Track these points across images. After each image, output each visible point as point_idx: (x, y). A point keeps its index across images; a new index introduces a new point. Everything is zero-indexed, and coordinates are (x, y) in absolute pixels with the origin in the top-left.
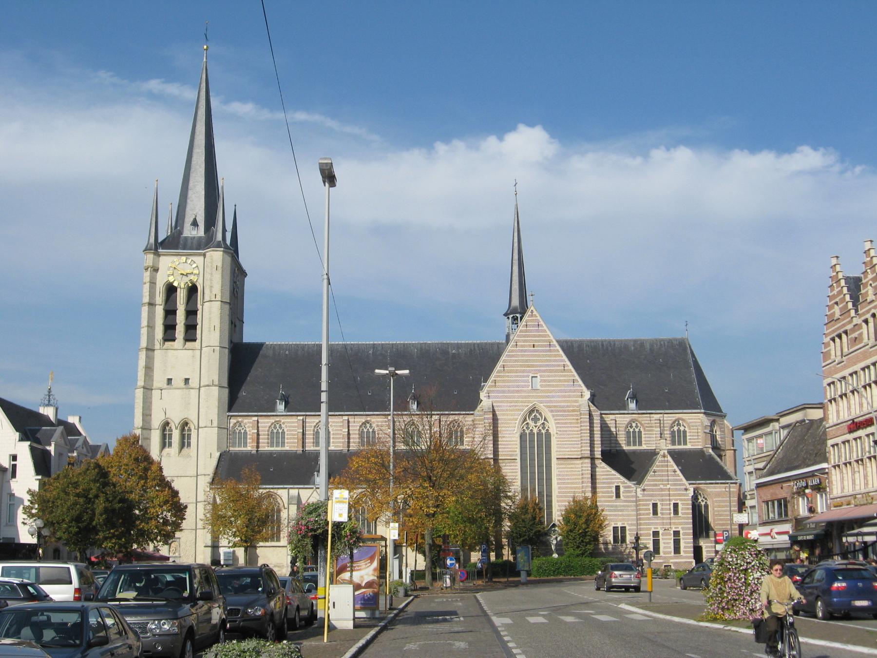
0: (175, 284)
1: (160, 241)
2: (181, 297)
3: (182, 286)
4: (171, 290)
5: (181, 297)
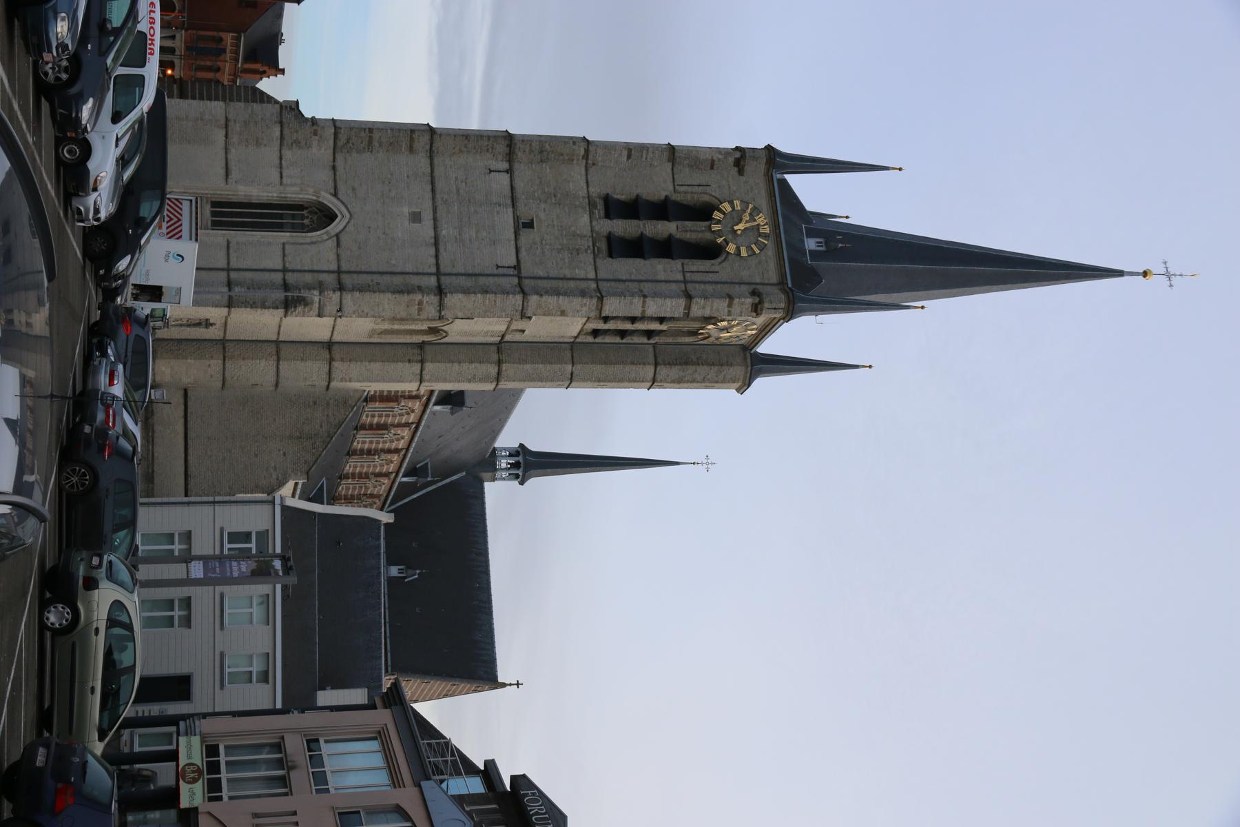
0: (717, 215)
1: (794, 180)
2: (689, 231)
3: (715, 228)
4: (703, 212)
5: (689, 231)
